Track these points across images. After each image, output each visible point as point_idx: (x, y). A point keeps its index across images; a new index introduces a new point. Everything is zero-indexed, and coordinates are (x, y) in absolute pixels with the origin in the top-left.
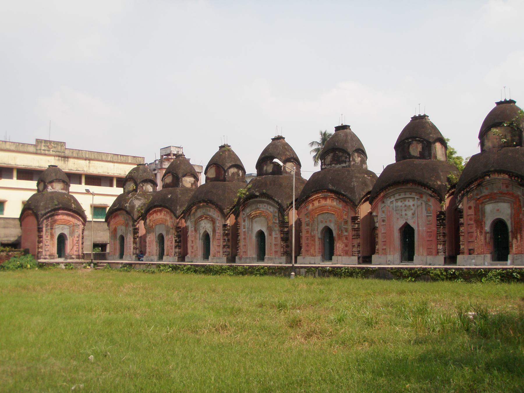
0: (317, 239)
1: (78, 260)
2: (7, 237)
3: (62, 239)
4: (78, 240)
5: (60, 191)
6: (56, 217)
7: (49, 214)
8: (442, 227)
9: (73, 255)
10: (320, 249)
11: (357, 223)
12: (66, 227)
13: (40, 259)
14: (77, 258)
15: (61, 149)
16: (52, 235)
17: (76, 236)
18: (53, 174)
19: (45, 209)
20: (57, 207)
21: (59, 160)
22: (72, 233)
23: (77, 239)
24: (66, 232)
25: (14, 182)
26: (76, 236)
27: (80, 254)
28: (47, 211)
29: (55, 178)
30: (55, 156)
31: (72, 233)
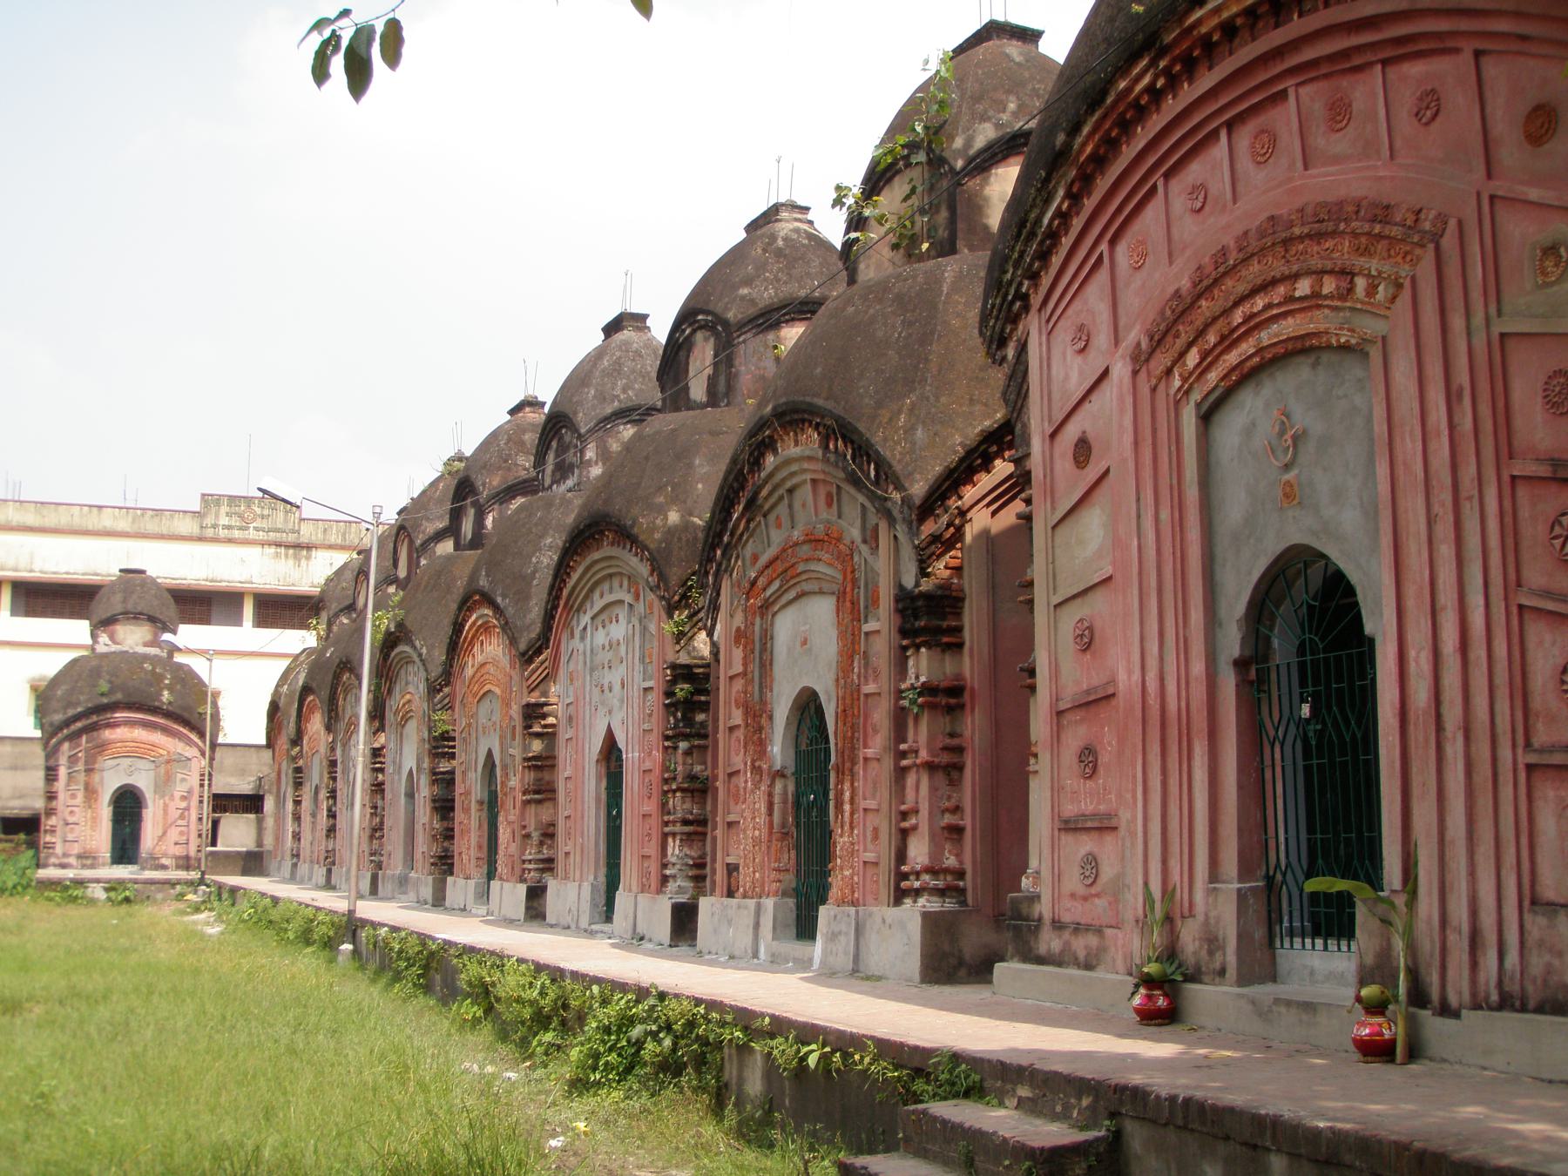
0: (474, 806)
1: (182, 875)
2: (20, 797)
3: (128, 806)
4: (187, 809)
5: (141, 650)
6: (107, 734)
7: (79, 725)
8: (683, 745)
9: (165, 855)
10: (480, 847)
11: (538, 735)
12: (142, 764)
13: (45, 866)
14: (178, 867)
15: (286, 521)
16: (91, 793)
17: (177, 795)
18: (119, 597)
19: (65, 708)
20: (105, 700)
21: (277, 555)
22: (164, 783)
23: (184, 805)
24: (143, 781)
25: (246, 633)
26: (177, 795)
27: (193, 853)
28: (71, 712)
29: (119, 608)
30: (263, 544)
31: (164, 783)
